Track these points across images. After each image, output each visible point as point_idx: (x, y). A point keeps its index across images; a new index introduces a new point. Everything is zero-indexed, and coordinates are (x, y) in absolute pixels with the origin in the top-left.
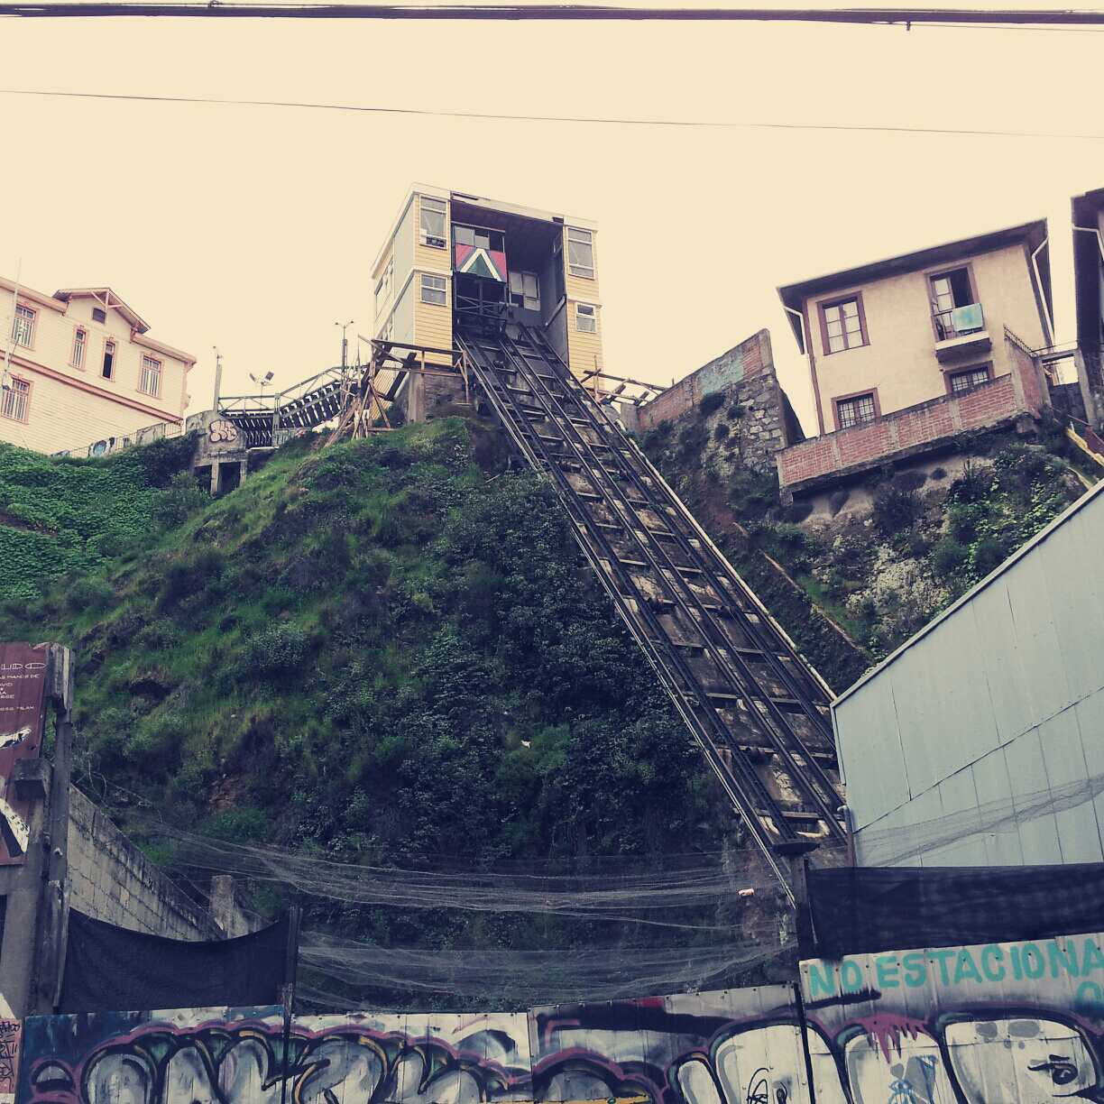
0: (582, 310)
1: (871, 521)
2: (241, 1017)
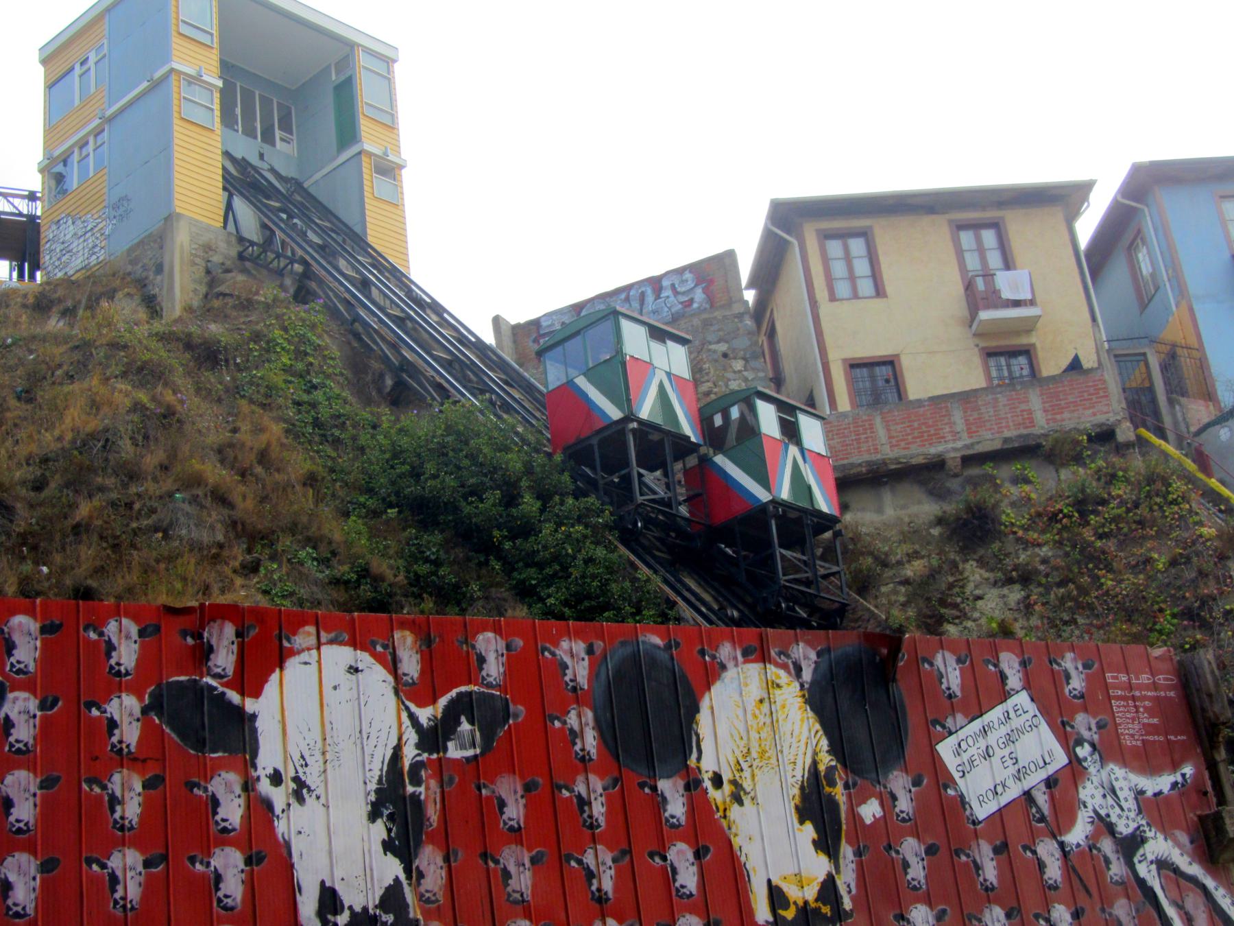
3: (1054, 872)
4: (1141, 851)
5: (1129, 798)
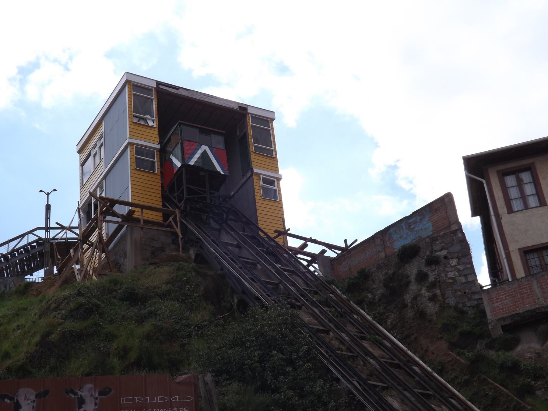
0: (266, 181)
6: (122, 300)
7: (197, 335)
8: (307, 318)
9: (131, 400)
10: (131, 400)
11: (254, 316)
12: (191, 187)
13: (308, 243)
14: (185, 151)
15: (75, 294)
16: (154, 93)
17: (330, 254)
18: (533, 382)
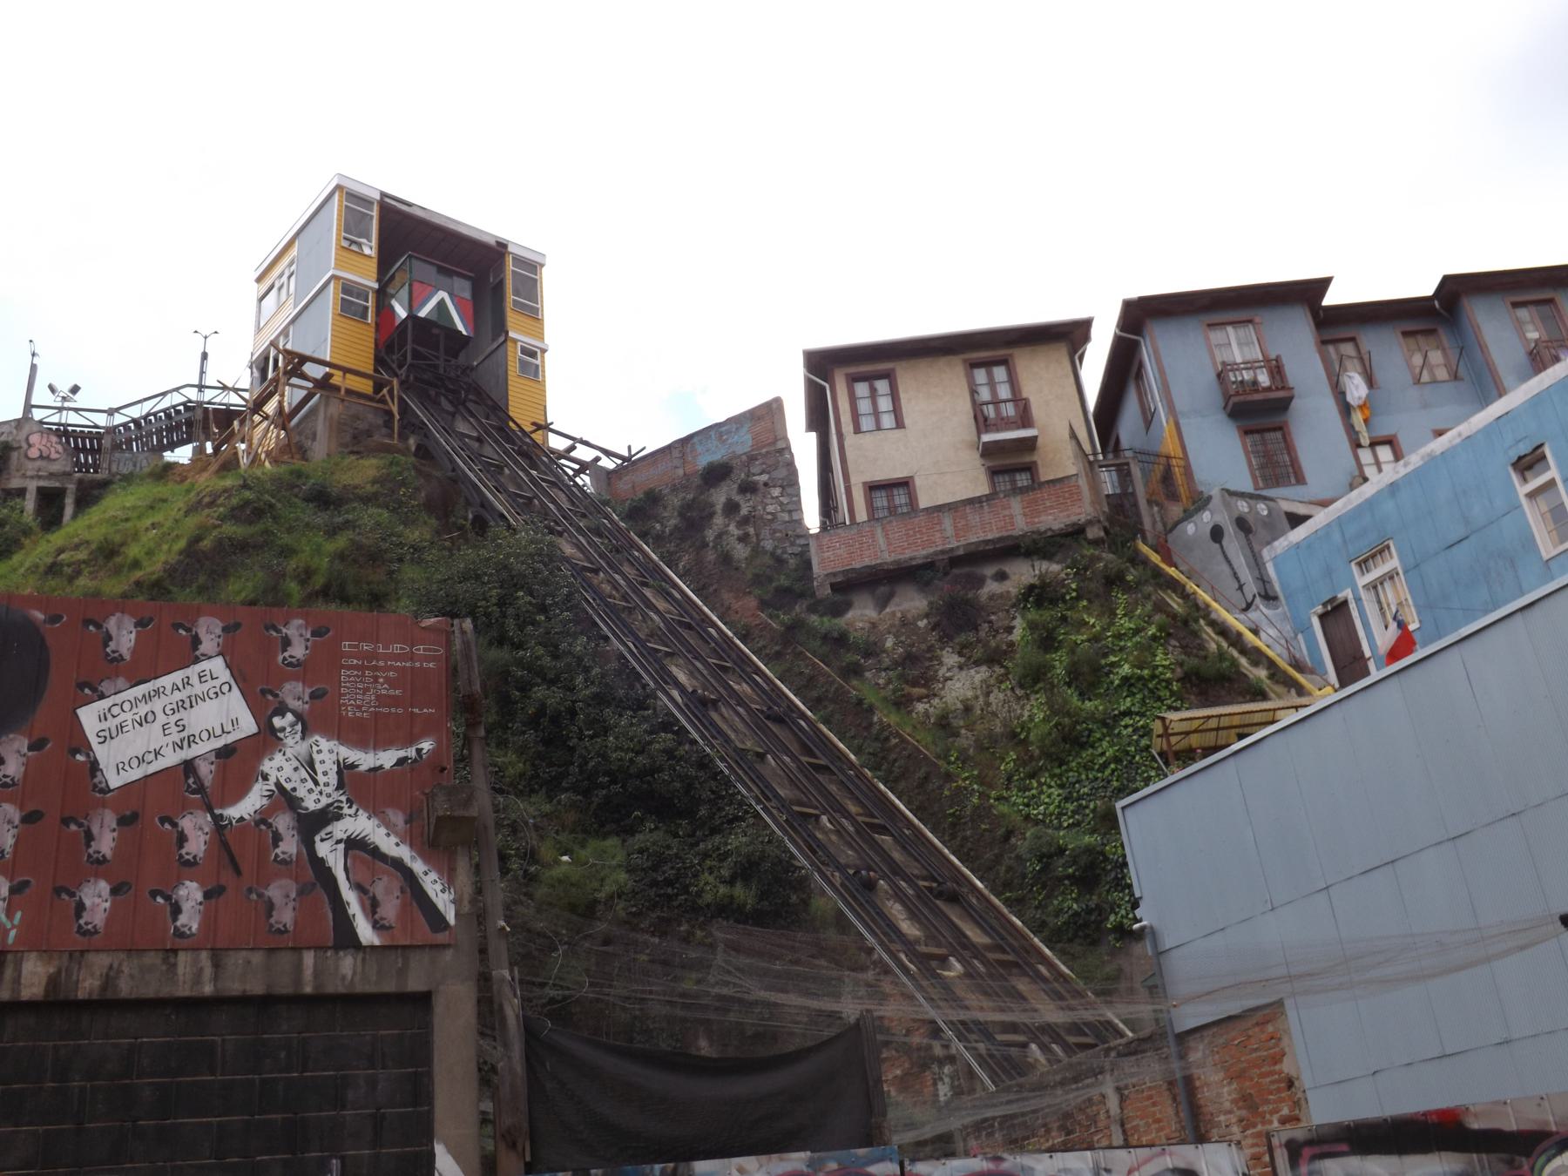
0: (525, 351)
1: (925, 621)
2: (833, 1166)
3: (196, 845)
4: (329, 829)
5: (330, 772)
6: (307, 500)
7: (412, 560)
8: (569, 550)
9: (356, 646)
10: (356, 646)
11: (495, 540)
12: (419, 348)
13: (577, 445)
14: (414, 295)
15: (240, 486)
16: (376, 208)
17: (608, 464)
18: (863, 661)
